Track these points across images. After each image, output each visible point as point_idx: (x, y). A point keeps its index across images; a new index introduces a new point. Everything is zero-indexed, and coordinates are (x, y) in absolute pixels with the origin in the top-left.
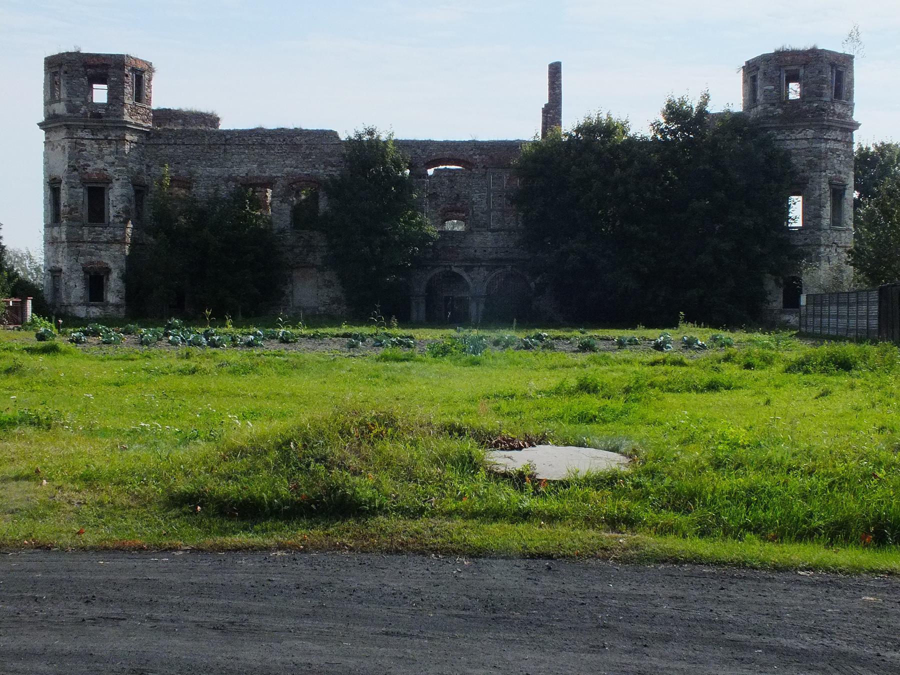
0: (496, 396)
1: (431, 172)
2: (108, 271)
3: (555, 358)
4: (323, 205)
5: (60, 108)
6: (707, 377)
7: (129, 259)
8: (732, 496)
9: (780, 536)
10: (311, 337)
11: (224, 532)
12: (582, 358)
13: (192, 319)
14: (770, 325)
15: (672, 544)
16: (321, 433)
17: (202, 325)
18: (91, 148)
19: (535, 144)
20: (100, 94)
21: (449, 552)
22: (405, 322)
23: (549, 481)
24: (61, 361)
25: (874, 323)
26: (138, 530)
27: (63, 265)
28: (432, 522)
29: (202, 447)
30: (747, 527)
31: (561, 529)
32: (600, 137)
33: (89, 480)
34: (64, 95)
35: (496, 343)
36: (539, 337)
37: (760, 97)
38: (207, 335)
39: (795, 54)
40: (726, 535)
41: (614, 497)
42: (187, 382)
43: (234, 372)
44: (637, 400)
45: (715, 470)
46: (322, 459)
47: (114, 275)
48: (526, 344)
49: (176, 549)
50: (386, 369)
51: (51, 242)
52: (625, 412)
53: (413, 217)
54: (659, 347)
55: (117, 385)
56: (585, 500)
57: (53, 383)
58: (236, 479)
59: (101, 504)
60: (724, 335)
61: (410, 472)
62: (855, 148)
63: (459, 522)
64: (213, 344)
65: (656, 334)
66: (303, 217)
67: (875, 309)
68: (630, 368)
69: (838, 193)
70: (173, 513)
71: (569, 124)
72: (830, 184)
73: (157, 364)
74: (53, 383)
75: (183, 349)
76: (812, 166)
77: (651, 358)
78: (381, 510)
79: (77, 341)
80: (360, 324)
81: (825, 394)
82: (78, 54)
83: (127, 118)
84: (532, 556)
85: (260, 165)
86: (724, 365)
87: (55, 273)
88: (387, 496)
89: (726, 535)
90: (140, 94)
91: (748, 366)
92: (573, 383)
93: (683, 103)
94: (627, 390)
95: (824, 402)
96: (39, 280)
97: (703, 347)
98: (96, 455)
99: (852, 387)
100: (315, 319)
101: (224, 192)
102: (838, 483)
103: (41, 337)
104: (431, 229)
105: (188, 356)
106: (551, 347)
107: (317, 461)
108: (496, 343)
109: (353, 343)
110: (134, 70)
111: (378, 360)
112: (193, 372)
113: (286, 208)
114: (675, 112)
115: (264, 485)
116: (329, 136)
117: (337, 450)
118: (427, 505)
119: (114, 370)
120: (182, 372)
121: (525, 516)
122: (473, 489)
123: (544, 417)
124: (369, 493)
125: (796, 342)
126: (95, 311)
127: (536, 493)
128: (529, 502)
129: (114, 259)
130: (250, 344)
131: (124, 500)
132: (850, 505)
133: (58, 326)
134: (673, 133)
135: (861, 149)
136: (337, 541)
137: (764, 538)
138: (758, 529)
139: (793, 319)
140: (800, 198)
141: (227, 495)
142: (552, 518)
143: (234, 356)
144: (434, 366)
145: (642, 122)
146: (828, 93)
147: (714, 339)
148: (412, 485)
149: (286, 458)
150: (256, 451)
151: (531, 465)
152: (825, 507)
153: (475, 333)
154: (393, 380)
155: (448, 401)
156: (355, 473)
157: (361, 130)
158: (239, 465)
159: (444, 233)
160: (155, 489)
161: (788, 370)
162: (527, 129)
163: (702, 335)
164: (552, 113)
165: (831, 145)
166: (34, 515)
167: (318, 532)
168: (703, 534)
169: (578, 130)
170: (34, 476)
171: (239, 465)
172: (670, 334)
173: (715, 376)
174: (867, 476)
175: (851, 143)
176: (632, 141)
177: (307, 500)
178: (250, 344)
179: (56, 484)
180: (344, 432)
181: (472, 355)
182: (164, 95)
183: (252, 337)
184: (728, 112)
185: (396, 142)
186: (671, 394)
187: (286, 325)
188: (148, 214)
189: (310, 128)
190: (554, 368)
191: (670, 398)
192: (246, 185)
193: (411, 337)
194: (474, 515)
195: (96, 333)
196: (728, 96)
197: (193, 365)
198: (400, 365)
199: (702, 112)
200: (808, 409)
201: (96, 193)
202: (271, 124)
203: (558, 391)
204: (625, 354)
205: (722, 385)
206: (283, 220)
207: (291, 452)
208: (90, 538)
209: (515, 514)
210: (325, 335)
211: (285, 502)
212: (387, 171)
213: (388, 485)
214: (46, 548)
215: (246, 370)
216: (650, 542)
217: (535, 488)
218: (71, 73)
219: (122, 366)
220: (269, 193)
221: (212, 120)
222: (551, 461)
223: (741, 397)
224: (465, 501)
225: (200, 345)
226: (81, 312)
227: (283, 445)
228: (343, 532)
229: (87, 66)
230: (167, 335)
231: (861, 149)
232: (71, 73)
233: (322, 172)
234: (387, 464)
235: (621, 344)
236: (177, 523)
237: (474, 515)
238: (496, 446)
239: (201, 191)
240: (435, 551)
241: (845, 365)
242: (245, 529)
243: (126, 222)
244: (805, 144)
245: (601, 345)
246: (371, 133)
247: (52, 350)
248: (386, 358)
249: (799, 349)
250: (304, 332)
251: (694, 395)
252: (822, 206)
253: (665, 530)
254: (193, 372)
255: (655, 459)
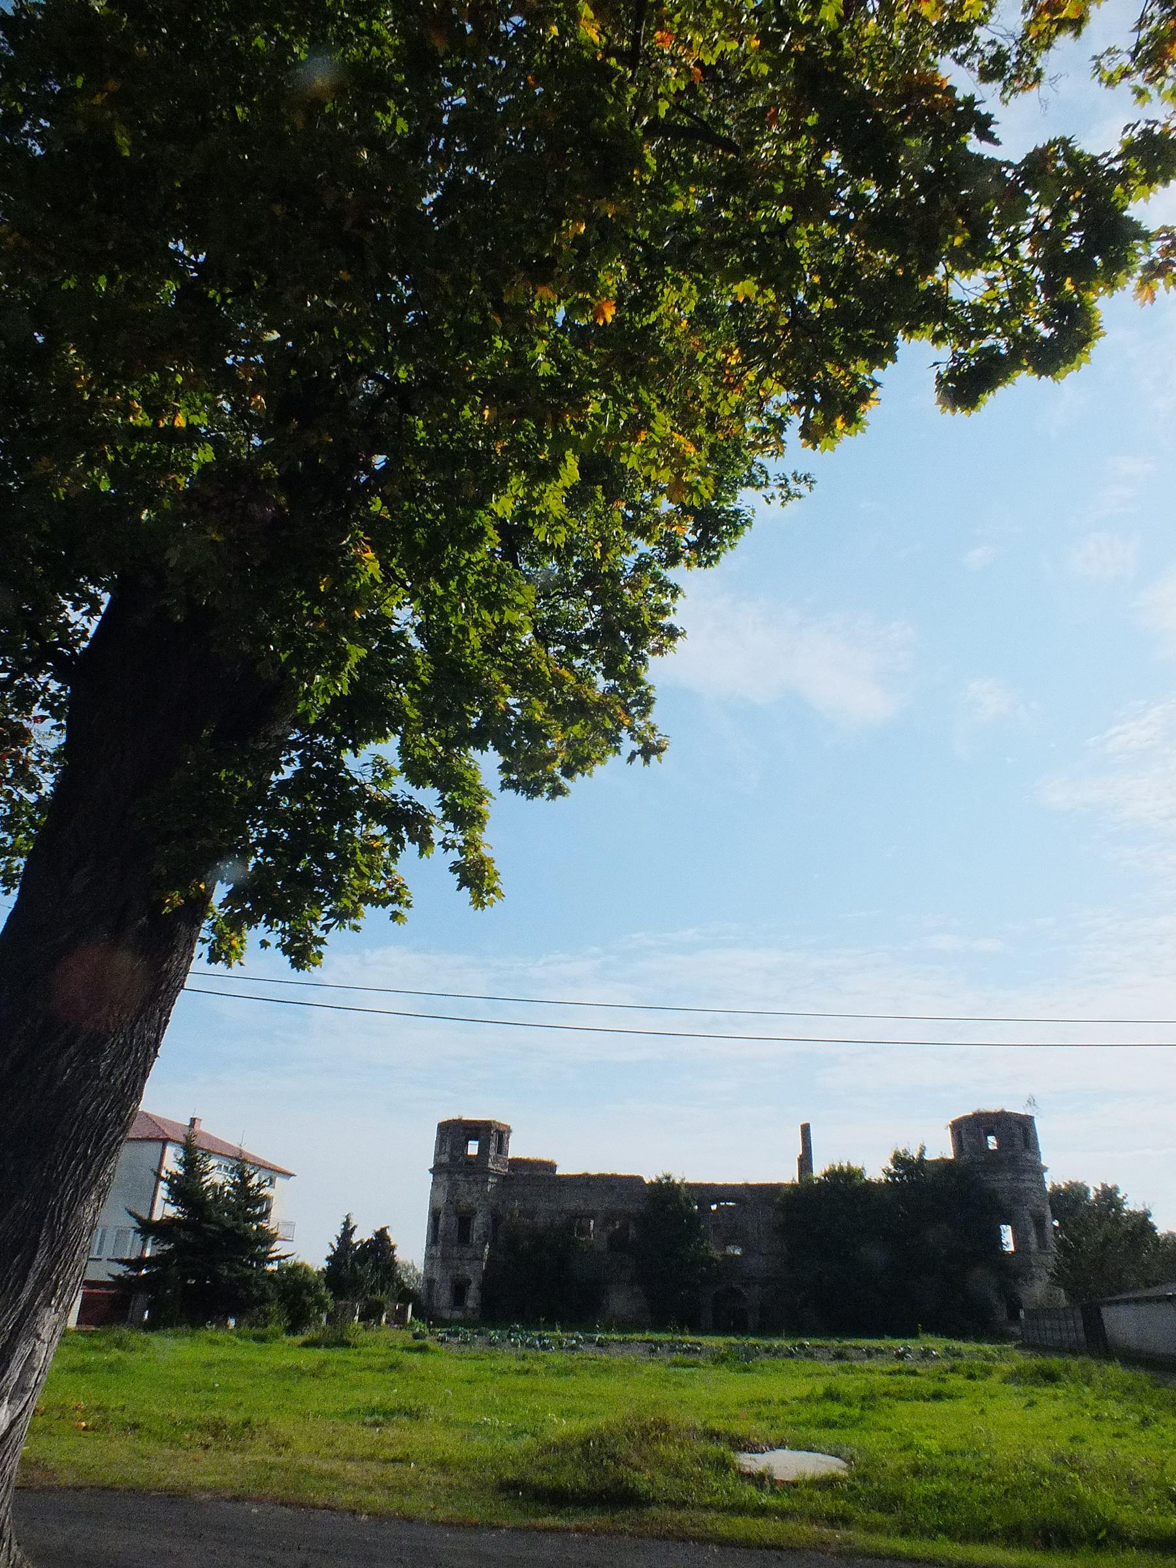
0: (759, 1401)
1: (714, 1207)
2: (470, 1283)
3: (808, 1366)
4: (632, 1232)
5: (445, 1159)
6: (933, 1386)
7: (485, 1273)
8: (926, 1500)
9: (965, 1538)
10: (621, 1343)
11: (537, 1515)
12: (834, 1366)
13: (530, 1323)
14: (996, 1335)
15: (882, 1542)
16: (612, 1435)
17: (538, 1329)
18: (463, 1187)
19: (793, 1186)
20: (473, 1148)
21: (704, 1541)
22: (696, 1329)
23: (783, 1482)
24: (430, 1359)
25: (1082, 1335)
26: (478, 1511)
27: (437, 1277)
28: (693, 1514)
29: (527, 1441)
30: (940, 1529)
31: (792, 1524)
32: (844, 1182)
33: (443, 1465)
34: (448, 1149)
35: (767, 1351)
36: (802, 1346)
37: (967, 1149)
38: (541, 1338)
39: (988, 1115)
40: (922, 1535)
41: (834, 1498)
42: (522, 1382)
43: (559, 1374)
44: (871, 1408)
45: (914, 1476)
46: (612, 1457)
47: (473, 1286)
48: (791, 1352)
49: (502, 1527)
50: (675, 1374)
51: (429, 1258)
52: (861, 1419)
53: (702, 1243)
54: (900, 1356)
55: (469, 1382)
56: (811, 1499)
57: (423, 1379)
58: (549, 1471)
59: (451, 1486)
60: (956, 1345)
61: (677, 1469)
62: (1048, 1187)
63: (712, 1515)
64: (544, 1347)
65: (899, 1344)
66: (617, 1242)
67: (1080, 1324)
68: (871, 1377)
69: (1040, 1222)
70: (503, 1495)
71: (819, 1170)
72: (1032, 1216)
73: (502, 1364)
74: (423, 1379)
75: (521, 1350)
76: (1016, 1201)
77: (891, 1367)
78: (653, 1501)
79: (442, 1340)
80: (658, 1331)
81: (1031, 1404)
82: (460, 1120)
83: (490, 1166)
84: (767, 1547)
85: (585, 1200)
86: (950, 1375)
87: (430, 1282)
88: (659, 1489)
89: (922, 1535)
90: (501, 1148)
91: (971, 1377)
92: (820, 1390)
93: (906, 1153)
94: (864, 1399)
95: (1030, 1412)
96: (417, 1286)
97: (937, 1357)
98: (448, 1443)
99: (1055, 1398)
100: (627, 1325)
101: (558, 1221)
102: (1012, 1491)
103: (416, 1336)
104: (716, 1254)
105: (524, 1358)
106: (810, 1355)
107: (609, 1457)
108: (767, 1351)
109: (653, 1348)
110: (497, 1131)
111: (669, 1366)
112: (527, 1372)
113: (605, 1235)
114: (900, 1160)
115: (573, 1477)
116: (635, 1182)
117: (621, 1450)
118: (689, 1499)
119: (467, 1368)
120: (518, 1372)
121: (762, 1511)
122: (720, 1487)
123: (781, 1421)
124: (645, 1486)
125: (1017, 1354)
126: (458, 1314)
127: (773, 1491)
128: (766, 1499)
129: (474, 1272)
130: (573, 1348)
131: (466, 1484)
132: (1023, 1512)
133: (429, 1326)
134: (901, 1176)
135: (1054, 1186)
136: (621, 1526)
137: (953, 1538)
138: (949, 1531)
139: (1016, 1329)
140: (1009, 1227)
141: (541, 1483)
142: (784, 1514)
143: (557, 1358)
144: (714, 1372)
145: (876, 1169)
146: (1019, 1143)
147: (947, 1349)
148: (678, 1481)
149: (586, 1453)
150: (563, 1446)
151: (770, 1468)
152: (1001, 1512)
153: (752, 1341)
154: (678, 1385)
155: (720, 1405)
156: (637, 1469)
157: (661, 1176)
158: (552, 1458)
159: (725, 1256)
160: (490, 1476)
161: (1005, 1381)
162: (786, 1174)
163: (937, 1344)
164: (805, 1162)
165: (1028, 1184)
166: (402, 1490)
167: (607, 1518)
168: (904, 1533)
169: (826, 1175)
170: (404, 1460)
171: (552, 1458)
172: (911, 1343)
173: (940, 1386)
174: (1036, 1484)
175: (1043, 1182)
176: (869, 1183)
177: (592, 1490)
178: (573, 1348)
179: (421, 1467)
180: (630, 1434)
181: (743, 1361)
182: (516, 1149)
183: (574, 1342)
184: (943, 1159)
185: (688, 1186)
186: (902, 1402)
187: (602, 1332)
188: (501, 1238)
189: (623, 1174)
190: (810, 1376)
191: (901, 1407)
192: (576, 1217)
193: (699, 1344)
194: (724, 1509)
195: (456, 1334)
196: (940, 1147)
197: (527, 1366)
198: (686, 1371)
199: (921, 1160)
200: (1016, 1418)
201: (465, 1221)
202: (594, 1171)
203: (808, 1399)
204: (868, 1364)
205: (946, 1395)
206: (602, 1246)
207: (593, 1449)
208: (441, 1514)
209: (755, 1509)
210: (633, 1341)
211: (583, 1491)
212: (681, 1207)
213: (661, 1481)
214: (410, 1520)
215: (565, 1372)
216: (860, 1538)
217: (772, 1487)
218: (454, 1134)
219: (472, 1366)
220: (592, 1223)
221: (551, 1166)
222: (787, 1464)
223: (963, 1406)
224: (718, 1496)
225: (534, 1346)
226: (447, 1315)
227: (585, 1443)
228: (625, 1519)
229: (466, 1128)
230: (509, 1337)
231: (1054, 1186)
232: (454, 1134)
233: (631, 1207)
234: (661, 1462)
235: (869, 1354)
236: (503, 1504)
237: (724, 1509)
238: (745, 1450)
239: (541, 1221)
240: (694, 1539)
241: (1051, 1377)
242: (554, 1513)
243: (485, 1244)
244: (1006, 1183)
245: (853, 1353)
246: (668, 1178)
247: (422, 1349)
248: (675, 1365)
249: (1020, 1359)
250: (616, 1337)
251: (921, 1403)
252: (1028, 1234)
253: (871, 1528)
254: (527, 1372)
255: (867, 1466)
